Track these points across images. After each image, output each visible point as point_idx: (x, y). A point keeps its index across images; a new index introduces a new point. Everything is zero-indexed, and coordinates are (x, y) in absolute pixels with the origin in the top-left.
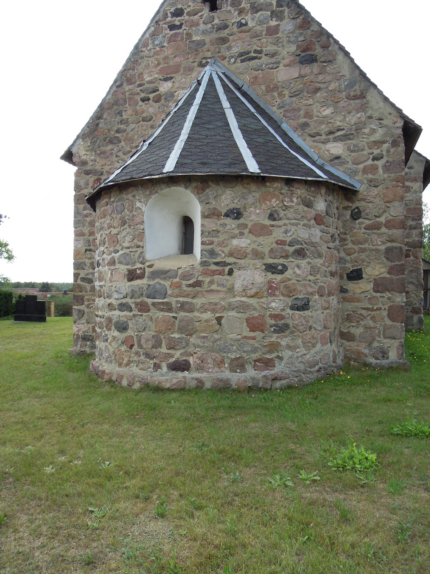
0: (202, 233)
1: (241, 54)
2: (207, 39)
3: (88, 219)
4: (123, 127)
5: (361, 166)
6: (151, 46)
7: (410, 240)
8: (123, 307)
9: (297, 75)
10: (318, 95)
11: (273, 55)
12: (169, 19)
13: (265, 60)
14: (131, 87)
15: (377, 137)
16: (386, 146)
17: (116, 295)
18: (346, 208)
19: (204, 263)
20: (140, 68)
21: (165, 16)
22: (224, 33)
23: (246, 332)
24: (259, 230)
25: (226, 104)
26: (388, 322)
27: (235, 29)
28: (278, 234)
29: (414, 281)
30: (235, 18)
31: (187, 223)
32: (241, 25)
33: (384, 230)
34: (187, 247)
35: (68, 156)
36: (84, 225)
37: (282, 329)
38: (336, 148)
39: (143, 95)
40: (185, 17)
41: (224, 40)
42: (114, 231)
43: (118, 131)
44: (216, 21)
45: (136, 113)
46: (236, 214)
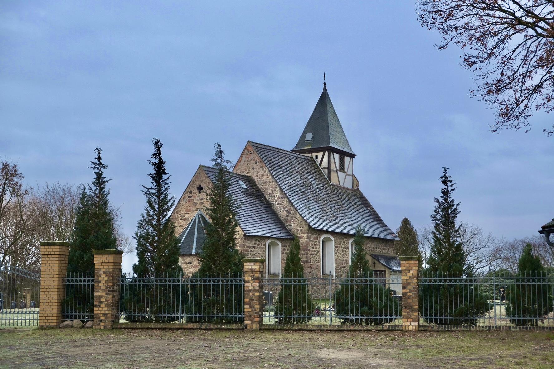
2: (198, 202)
20: (180, 209)
40: (192, 194)
46: (190, 263)
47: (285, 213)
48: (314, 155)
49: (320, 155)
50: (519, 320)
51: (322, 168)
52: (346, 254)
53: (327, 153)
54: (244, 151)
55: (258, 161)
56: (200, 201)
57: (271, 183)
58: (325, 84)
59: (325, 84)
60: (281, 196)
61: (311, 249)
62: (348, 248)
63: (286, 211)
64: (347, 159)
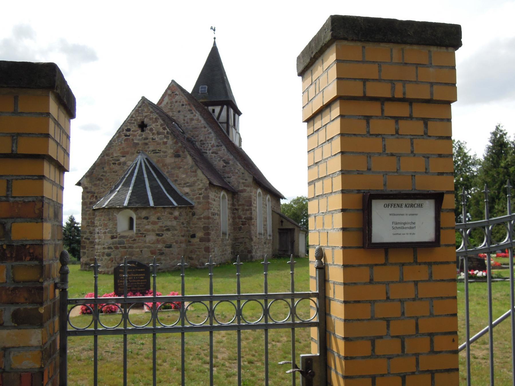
0: (136, 224)
1: (153, 151)
3: (88, 212)
4: (104, 174)
5: (195, 197)
6: (116, 142)
7: (246, 216)
8: (109, 248)
9: (173, 161)
10: (181, 169)
11: (165, 152)
12: (125, 132)
13: (162, 154)
14: (108, 157)
15: (200, 187)
16: (203, 190)
17: (106, 244)
18: (190, 212)
19: (136, 234)
21: (123, 130)
22: (147, 141)
23: (150, 255)
24: (154, 223)
25: (145, 176)
26: (204, 253)
27: (151, 140)
28: (160, 224)
29: (248, 237)
30: (151, 136)
31: (131, 219)
32: (153, 139)
33: (203, 220)
34: (131, 227)
35: (79, 184)
36: (86, 215)
37: (162, 254)
38: (187, 190)
39: (113, 162)
40: (131, 132)
41: (146, 144)
42: (106, 222)
43: (102, 175)
44: (144, 136)
45: (110, 169)
46: (147, 218)
47: (222, 163)
48: (210, 108)
49: (217, 109)
51: (221, 123)
53: (225, 107)
54: (166, 91)
55: (185, 103)
56: (143, 141)
57: (203, 129)
58: (215, 38)
59: (215, 38)
60: (216, 144)
63: (224, 161)
64: (237, 115)
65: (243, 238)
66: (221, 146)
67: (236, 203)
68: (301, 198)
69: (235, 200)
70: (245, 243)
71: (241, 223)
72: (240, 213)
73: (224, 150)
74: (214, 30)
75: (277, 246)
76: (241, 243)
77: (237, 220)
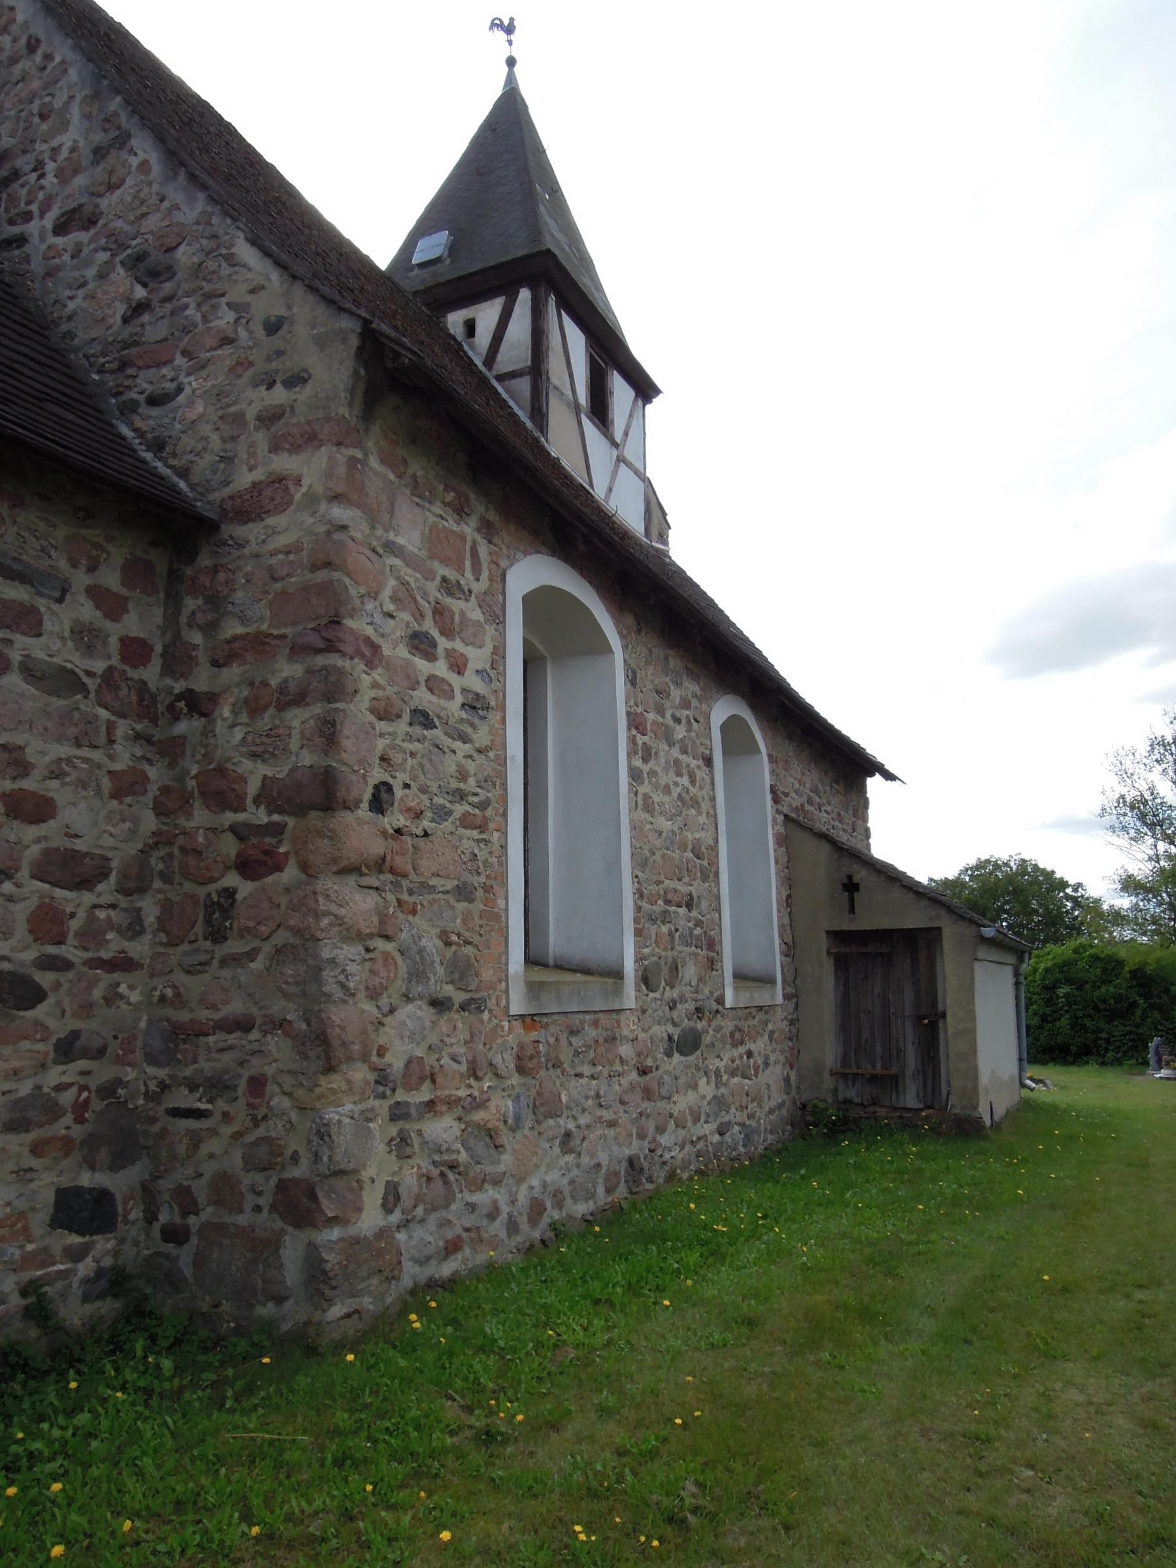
7: (279, 771)
48: (455, 320)
49: (487, 315)
50: (548, 1165)
51: (500, 378)
52: (695, 803)
53: (525, 295)
58: (511, 62)
59: (511, 62)
61: (397, 651)
62: (709, 761)
65: (243, 1025)
66: (122, 140)
67: (197, 638)
68: (988, 861)
69: (191, 604)
70: (257, 1084)
71: (230, 847)
72: (230, 733)
73: (144, 166)
74: (509, 29)
75: (828, 1050)
76: (218, 1086)
77: (200, 817)
